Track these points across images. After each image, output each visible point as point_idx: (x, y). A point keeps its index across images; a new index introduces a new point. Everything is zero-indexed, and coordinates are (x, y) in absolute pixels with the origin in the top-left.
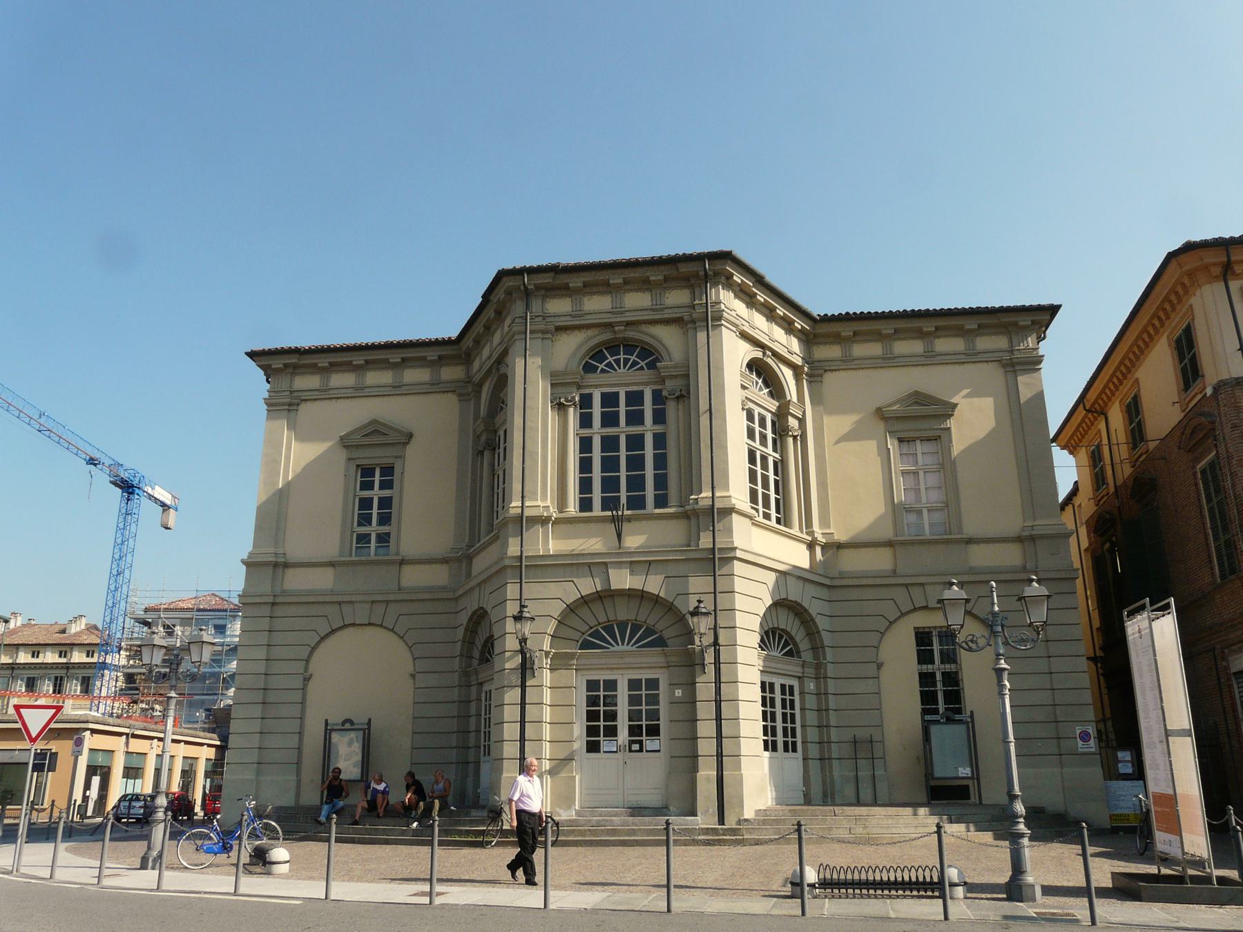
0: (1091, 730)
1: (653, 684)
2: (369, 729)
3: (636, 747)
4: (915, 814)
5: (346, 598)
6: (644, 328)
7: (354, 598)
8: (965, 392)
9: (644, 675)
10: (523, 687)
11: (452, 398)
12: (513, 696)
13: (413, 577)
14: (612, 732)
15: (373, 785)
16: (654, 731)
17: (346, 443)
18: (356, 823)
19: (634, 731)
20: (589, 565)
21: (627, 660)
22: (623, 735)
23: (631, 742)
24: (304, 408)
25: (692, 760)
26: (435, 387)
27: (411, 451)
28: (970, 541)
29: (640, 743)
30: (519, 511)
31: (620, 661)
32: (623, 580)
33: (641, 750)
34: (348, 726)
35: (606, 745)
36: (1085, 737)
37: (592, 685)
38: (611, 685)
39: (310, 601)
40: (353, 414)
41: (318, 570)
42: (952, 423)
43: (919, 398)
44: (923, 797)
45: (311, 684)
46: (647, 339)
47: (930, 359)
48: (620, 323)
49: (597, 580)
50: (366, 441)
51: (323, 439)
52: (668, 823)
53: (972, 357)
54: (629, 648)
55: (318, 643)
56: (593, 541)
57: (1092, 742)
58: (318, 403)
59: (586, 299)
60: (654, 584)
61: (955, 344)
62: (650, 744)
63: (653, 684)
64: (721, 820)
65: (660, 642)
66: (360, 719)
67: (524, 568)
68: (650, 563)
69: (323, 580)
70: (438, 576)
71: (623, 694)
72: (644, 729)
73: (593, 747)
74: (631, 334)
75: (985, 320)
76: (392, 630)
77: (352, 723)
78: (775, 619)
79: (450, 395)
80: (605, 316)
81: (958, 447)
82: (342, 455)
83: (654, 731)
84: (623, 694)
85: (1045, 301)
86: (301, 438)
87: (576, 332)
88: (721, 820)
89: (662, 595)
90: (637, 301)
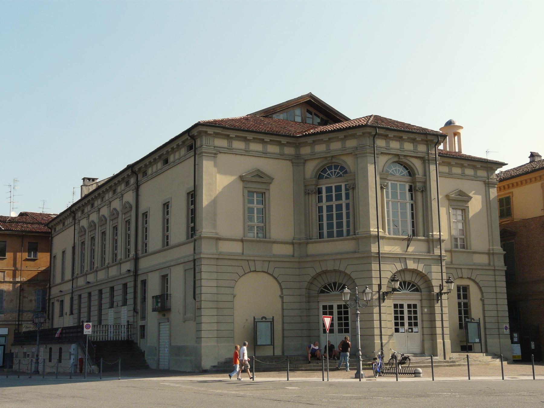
0: (508, 326)
1: (415, 306)
2: (273, 321)
3: (410, 330)
4: (57, 378)
5: (252, 258)
6: (408, 158)
7: (255, 258)
8: (473, 192)
9: (412, 303)
10: (380, 306)
11: (289, 163)
12: (376, 310)
13: (278, 250)
14: (403, 324)
15: (312, 346)
16: (416, 324)
17: (241, 178)
18: (310, 363)
19: (410, 324)
20: (400, 258)
21: (408, 296)
22: (406, 326)
23: (409, 328)
24: (220, 156)
25: (433, 335)
26: (281, 156)
27: (272, 187)
28: (475, 253)
29: (412, 329)
30: (377, 233)
31: (406, 297)
32: (411, 265)
33: (412, 332)
34: (264, 320)
35: (401, 330)
36: (506, 328)
37: (396, 306)
38: (402, 306)
39: (231, 258)
40: (247, 164)
41: (234, 243)
42: (470, 204)
43: (461, 193)
44: (460, 349)
45: (235, 298)
46: (410, 164)
47: (463, 176)
48: (402, 155)
49: (402, 264)
50: (254, 179)
51: (232, 175)
52: (467, 356)
53: (475, 178)
54: (408, 292)
55: (277, 281)
56: (397, 247)
57: (508, 330)
58: (226, 155)
59: (391, 142)
60: (421, 268)
61: (469, 172)
62: (415, 329)
63: (415, 306)
64: (445, 359)
65: (417, 290)
66: (269, 317)
67: (379, 257)
68: (419, 259)
69: (236, 248)
70: (288, 250)
71: (406, 309)
72: (413, 323)
73: (397, 330)
74: (404, 160)
75: (483, 165)
76: (245, 274)
77: (266, 319)
78: (403, 277)
79: (288, 161)
80: (396, 151)
81: (471, 214)
82: (240, 185)
83: (416, 324)
84: (406, 309)
85: (491, 157)
86: (220, 172)
87: (385, 155)
88: (445, 359)
89: (423, 272)
90: (408, 146)
